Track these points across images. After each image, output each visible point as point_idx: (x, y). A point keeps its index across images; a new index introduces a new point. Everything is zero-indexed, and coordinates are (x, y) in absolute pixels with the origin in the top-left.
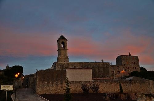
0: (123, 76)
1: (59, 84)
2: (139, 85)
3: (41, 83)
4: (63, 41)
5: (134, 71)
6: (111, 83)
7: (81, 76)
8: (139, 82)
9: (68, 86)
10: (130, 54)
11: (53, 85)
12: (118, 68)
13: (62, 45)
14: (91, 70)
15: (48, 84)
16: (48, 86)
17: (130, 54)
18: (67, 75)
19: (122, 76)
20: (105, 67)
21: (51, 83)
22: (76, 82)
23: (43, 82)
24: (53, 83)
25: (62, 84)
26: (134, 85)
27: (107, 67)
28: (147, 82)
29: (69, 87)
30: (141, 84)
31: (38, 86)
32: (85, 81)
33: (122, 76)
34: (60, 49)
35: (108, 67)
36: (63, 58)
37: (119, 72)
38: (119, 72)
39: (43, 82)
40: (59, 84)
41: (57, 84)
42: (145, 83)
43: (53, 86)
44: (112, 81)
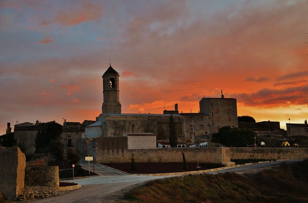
0: (208, 133)
1: (120, 152)
2: (209, 153)
3: (101, 151)
4: (112, 77)
5: (224, 127)
6: (178, 152)
7: (143, 143)
8: (210, 151)
9: (133, 156)
10: (222, 96)
11: (113, 153)
12: (201, 119)
13: (111, 82)
14: (156, 136)
15: (109, 152)
16: (108, 154)
17: (222, 96)
18: (128, 143)
19: (206, 133)
20: (177, 123)
21: (111, 151)
22: (138, 150)
23: (103, 150)
24: (113, 151)
25: (123, 152)
26: (204, 153)
27: (179, 123)
28: (219, 149)
29: (134, 157)
30: (212, 152)
31: (98, 155)
32: (148, 149)
33: (206, 133)
34: (108, 91)
35: (182, 123)
36: (112, 104)
37: (203, 125)
38: (201, 127)
39: (103, 150)
40: (120, 152)
41: (118, 152)
42: (216, 151)
43: (113, 155)
44: (179, 149)
